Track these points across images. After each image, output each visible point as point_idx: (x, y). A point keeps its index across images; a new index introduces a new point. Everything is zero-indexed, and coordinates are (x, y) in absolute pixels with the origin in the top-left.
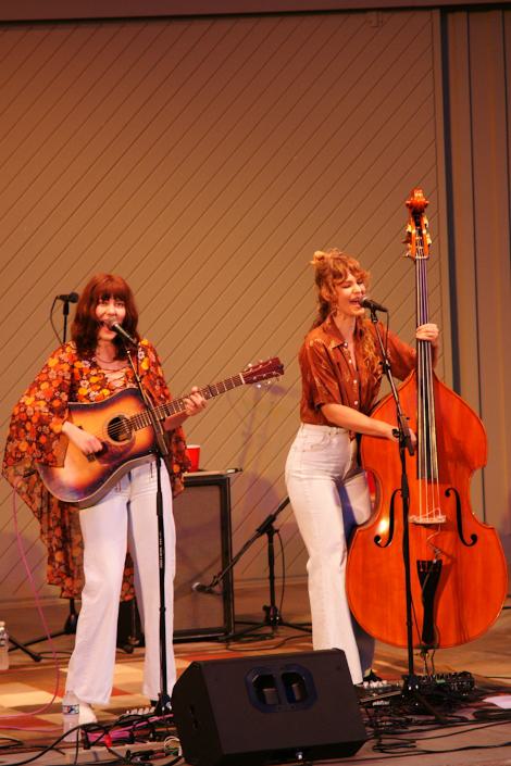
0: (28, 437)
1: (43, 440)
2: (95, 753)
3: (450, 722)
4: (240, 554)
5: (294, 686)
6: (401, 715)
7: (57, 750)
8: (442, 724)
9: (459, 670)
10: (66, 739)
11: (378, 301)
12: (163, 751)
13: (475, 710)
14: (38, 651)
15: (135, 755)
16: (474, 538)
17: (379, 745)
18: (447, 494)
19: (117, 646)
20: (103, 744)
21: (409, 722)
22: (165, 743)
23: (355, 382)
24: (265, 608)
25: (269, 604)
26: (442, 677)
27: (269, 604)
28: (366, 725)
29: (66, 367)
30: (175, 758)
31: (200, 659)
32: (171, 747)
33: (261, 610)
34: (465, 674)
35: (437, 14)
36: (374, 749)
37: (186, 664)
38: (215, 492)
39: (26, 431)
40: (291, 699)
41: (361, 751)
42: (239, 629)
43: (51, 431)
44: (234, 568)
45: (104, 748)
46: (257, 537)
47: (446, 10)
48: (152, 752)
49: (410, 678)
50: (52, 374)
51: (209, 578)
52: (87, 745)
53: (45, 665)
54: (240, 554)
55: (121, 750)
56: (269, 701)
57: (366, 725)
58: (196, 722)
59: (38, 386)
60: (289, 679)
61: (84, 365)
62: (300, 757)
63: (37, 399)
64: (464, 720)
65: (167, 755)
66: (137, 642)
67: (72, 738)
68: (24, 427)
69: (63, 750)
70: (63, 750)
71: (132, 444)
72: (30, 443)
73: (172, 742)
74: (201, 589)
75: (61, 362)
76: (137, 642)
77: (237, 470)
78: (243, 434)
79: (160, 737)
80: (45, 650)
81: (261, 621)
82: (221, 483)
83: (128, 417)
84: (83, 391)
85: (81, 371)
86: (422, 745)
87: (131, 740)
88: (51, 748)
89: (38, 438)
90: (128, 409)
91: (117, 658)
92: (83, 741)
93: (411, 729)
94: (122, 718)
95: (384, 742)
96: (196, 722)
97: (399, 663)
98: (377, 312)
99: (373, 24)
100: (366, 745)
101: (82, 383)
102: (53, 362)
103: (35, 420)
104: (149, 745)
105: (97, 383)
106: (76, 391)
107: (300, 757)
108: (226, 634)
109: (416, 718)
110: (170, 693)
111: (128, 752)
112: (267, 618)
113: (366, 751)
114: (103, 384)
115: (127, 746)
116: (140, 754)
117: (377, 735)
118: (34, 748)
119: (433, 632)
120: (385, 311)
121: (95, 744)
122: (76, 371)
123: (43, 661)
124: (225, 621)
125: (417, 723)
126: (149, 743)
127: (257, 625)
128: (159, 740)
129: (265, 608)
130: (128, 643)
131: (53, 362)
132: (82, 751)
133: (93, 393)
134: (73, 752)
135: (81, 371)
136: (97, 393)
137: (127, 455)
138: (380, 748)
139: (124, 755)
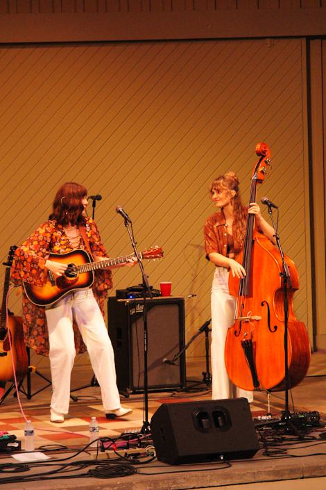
0: (24, 269)
1: (34, 272)
2: (107, 454)
3: (306, 439)
4: (189, 344)
5: (219, 418)
6: (279, 435)
7: (86, 452)
8: (301, 440)
9: (313, 410)
10: (91, 446)
11: (274, 202)
12: (145, 453)
13: (320, 433)
14: (76, 396)
15: (129, 455)
16: (276, 328)
17: (266, 452)
18: (263, 305)
19: (120, 393)
20: (112, 449)
21: (283, 439)
22: (147, 449)
23: (225, 246)
24: (203, 374)
25: (205, 371)
26: (302, 414)
27: (205, 371)
28: (259, 440)
29: (49, 235)
30: (152, 457)
31: (167, 402)
32: (150, 451)
33: (201, 374)
34: (315, 412)
35: (304, 40)
36: (264, 454)
37: (159, 405)
38: (175, 309)
39: (24, 266)
40: (217, 425)
41: (255, 456)
42: (188, 385)
43: (39, 268)
44: (186, 351)
45: (113, 451)
46: (200, 333)
47: (309, 38)
48: (139, 454)
49: (286, 413)
50: (40, 238)
51: (171, 358)
52: (103, 449)
53: (80, 403)
54: (189, 344)
55: (122, 452)
56: (205, 426)
57: (259, 440)
58: (164, 437)
59: (32, 243)
62: (222, 458)
63: (30, 249)
64: (314, 438)
65: (148, 455)
66: (131, 391)
67: (95, 445)
68: (23, 264)
69: (90, 452)
70: (90, 452)
71: (76, 280)
72: (26, 273)
73: (151, 449)
74: (167, 362)
75: (46, 232)
76: (131, 391)
77: (193, 296)
78: (193, 275)
79: (144, 445)
80: (79, 395)
81: (201, 381)
82: (179, 303)
83: (77, 265)
84: (57, 248)
85: (56, 238)
86: (291, 452)
87: (127, 447)
88: (83, 451)
89: (31, 270)
90: (77, 261)
91: (121, 400)
92: (101, 447)
93: (284, 443)
94: (123, 434)
95: (269, 450)
96: (164, 437)
97: (280, 406)
98: (272, 208)
99: (269, 45)
100: (259, 451)
101: (56, 244)
102: (42, 231)
103: (29, 260)
104: (138, 450)
105: (64, 245)
106: (53, 247)
107: (222, 458)
108: (181, 388)
109: (287, 437)
110: (149, 421)
111: (126, 454)
112: (204, 379)
113: (258, 456)
114: (68, 244)
115: (125, 450)
116: (132, 455)
117: (265, 446)
118: (73, 450)
119: (258, 382)
120: (276, 208)
121: (107, 449)
122: (54, 237)
123: (79, 401)
124: (181, 381)
125: (288, 440)
126: (137, 449)
127: (199, 383)
128: (143, 448)
129: (203, 374)
130: (126, 391)
131: (42, 231)
132: (100, 453)
133: (62, 250)
134: (95, 453)
135: (56, 238)
136: (64, 251)
137: (73, 286)
138: (267, 454)
139: (123, 455)
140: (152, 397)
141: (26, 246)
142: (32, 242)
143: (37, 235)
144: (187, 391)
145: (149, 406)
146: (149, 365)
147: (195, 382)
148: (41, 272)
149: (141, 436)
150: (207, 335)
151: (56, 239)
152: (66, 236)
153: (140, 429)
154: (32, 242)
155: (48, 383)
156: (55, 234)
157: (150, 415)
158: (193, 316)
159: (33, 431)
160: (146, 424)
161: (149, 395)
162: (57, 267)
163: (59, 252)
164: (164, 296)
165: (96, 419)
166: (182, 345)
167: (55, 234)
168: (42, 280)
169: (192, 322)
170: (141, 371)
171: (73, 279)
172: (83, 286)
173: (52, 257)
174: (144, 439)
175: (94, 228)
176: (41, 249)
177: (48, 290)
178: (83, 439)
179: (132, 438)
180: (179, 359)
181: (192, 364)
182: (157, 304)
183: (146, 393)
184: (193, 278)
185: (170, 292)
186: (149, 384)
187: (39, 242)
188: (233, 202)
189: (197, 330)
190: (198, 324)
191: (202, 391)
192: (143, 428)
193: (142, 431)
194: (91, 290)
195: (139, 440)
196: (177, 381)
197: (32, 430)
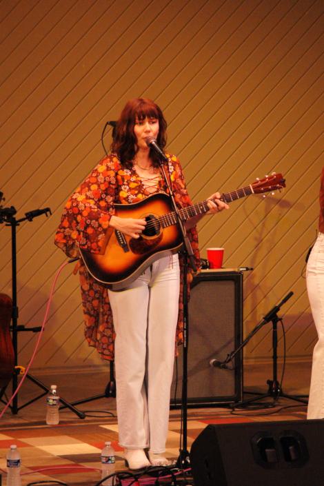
5: (291, 448)
25: (272, 379)
27: (272, 379)
29: (112, 174)
31: (215, 422)
33: (265, 383)
37: (203, 426)
38: (230, 287)
40: (287, 457)
42: (247, 398)
44: (244, 348)
46: (264, 323)
53: (89, 421)
59: (89, 187)
60: (286, 442)
61: (126, 173)
63: (88, 198)
71: (160, 238)
75: (108, 169)
78: (256, 239)
82: (235, 278)
83: (157, 217)
84: (123, 194)
89: (86, 229)
90: (157, 211)
103: (85, 213)
105: (135, 189)
108: (237, 402)
110: (189, 449)
112: (271, 389)
114: (140, 188)
122: (119, 177)
123: (87, 418)
127: (260, 395)
131: (101, 168)
136: (134, 197)
140: (193, 415)
141: (80, 193)
142: (88, 185)
143: (94, 175)
144: (244, 406)
145: (189, 427)
146: (189, 368)
147: (256, 394)
148: (100, 233)
149: (176, 471)
150: (275, 327)
151: (123, 181)
152: (138, 176)
153: (175, 461)
154: (88, 185)
155: (43, 391)
156: (120, 172)
157: (190, 440)
158: (254, 297)
159: (19, 461)
160: (184, 453)
161: (189, 411)
162: (131, 223)
163: (126, 199)
164: (213, 268)
165: (111, 445)
166: (239, 340)
167: (120, 172)
168: (100, 244)
169: (254, 309)
170: (179, 376)
171: (155, 237)
172: (170, 246)
173: (121, 209)
174: (181, 475)
175: (178, 170)
176: (104, 196)
177: (115, 258)
178: (90, 473)
179: (163, 474)
180: (233, 360)
181: (253, 369)
182: (204, 281)
183: (185, 408)
184: (256, 243)
185: (221, 264)
186: (190, 395)
187: (99, 186)
188: (154, 121)
189: (261, 318)
190: (262, 312)
191: (266, 407)
192: (179, 460)
193: (178, 465)
194: (176, 257)
195: (174, 477)
196: (229, 391)
197: (18, 459)
